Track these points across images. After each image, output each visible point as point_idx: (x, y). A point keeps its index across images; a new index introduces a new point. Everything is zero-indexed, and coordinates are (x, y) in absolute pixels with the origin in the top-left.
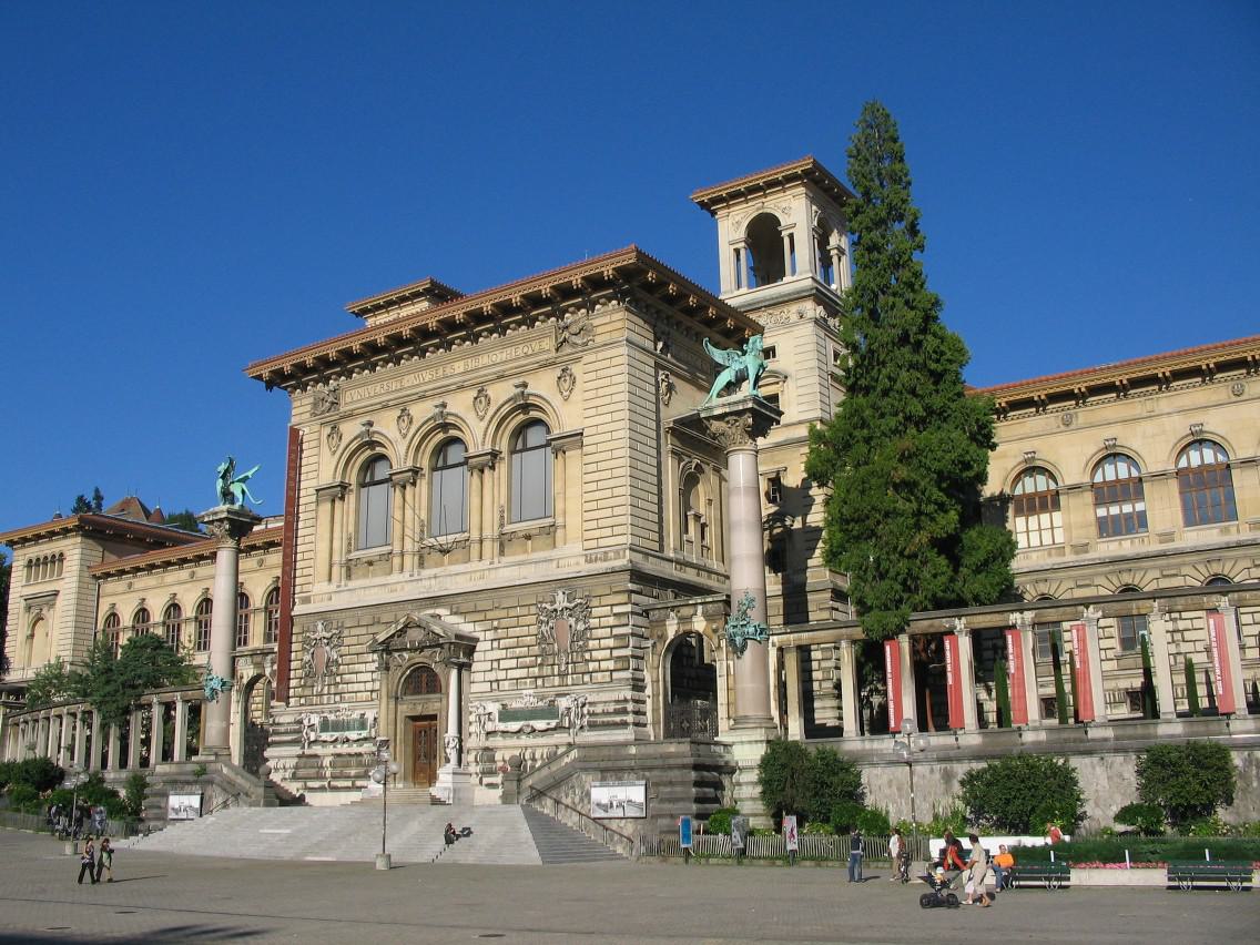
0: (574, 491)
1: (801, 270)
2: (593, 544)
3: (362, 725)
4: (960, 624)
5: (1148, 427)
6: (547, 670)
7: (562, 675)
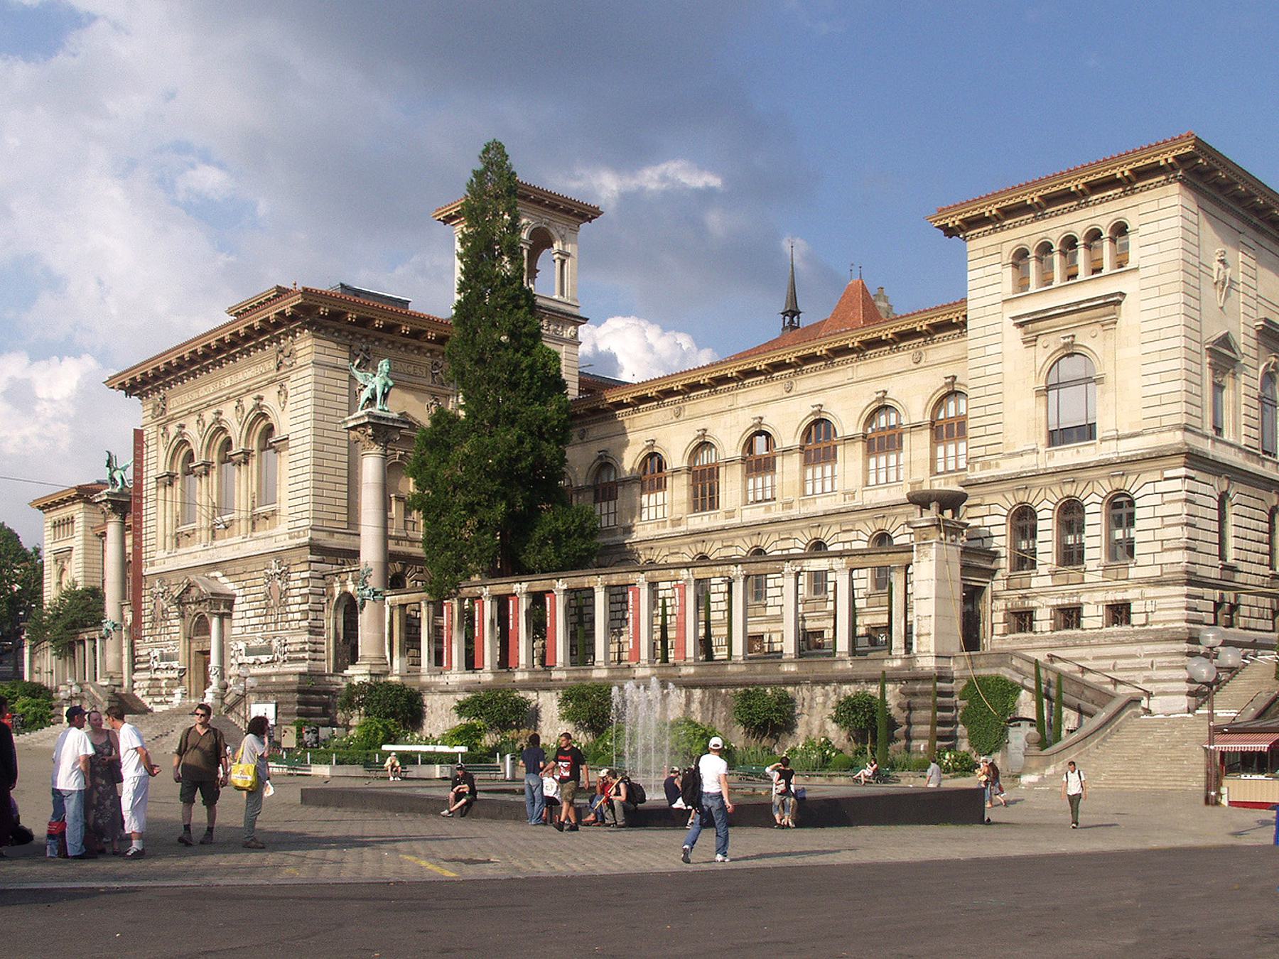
5: (728, 418)
6: (269, 619)
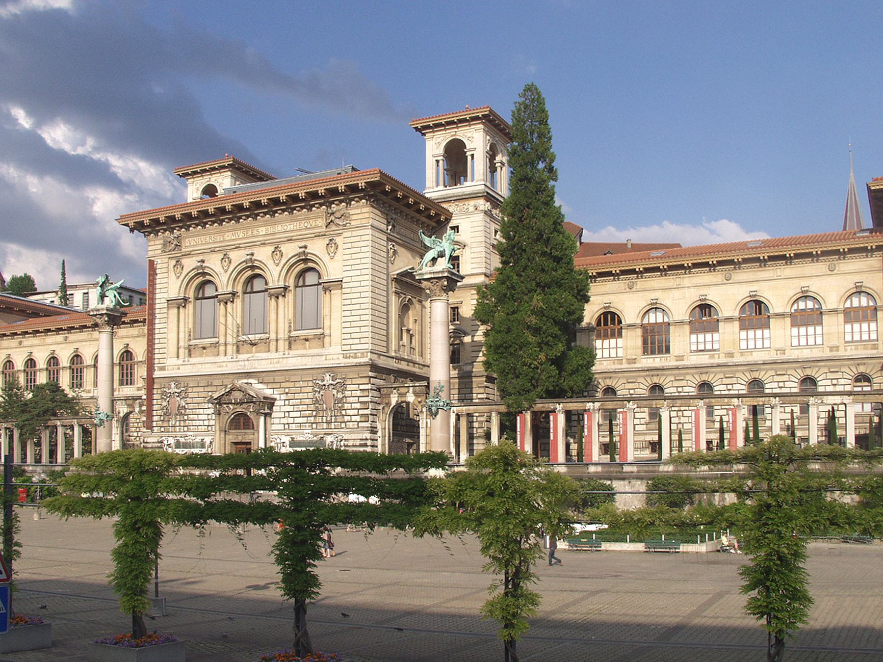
0: (336, 314)
1: (477, 178)
2: (348, 347)
3: (203, 446)
4: (559, 407)
5: (677, 293)
6: (319, 419)
7: (328, 423)
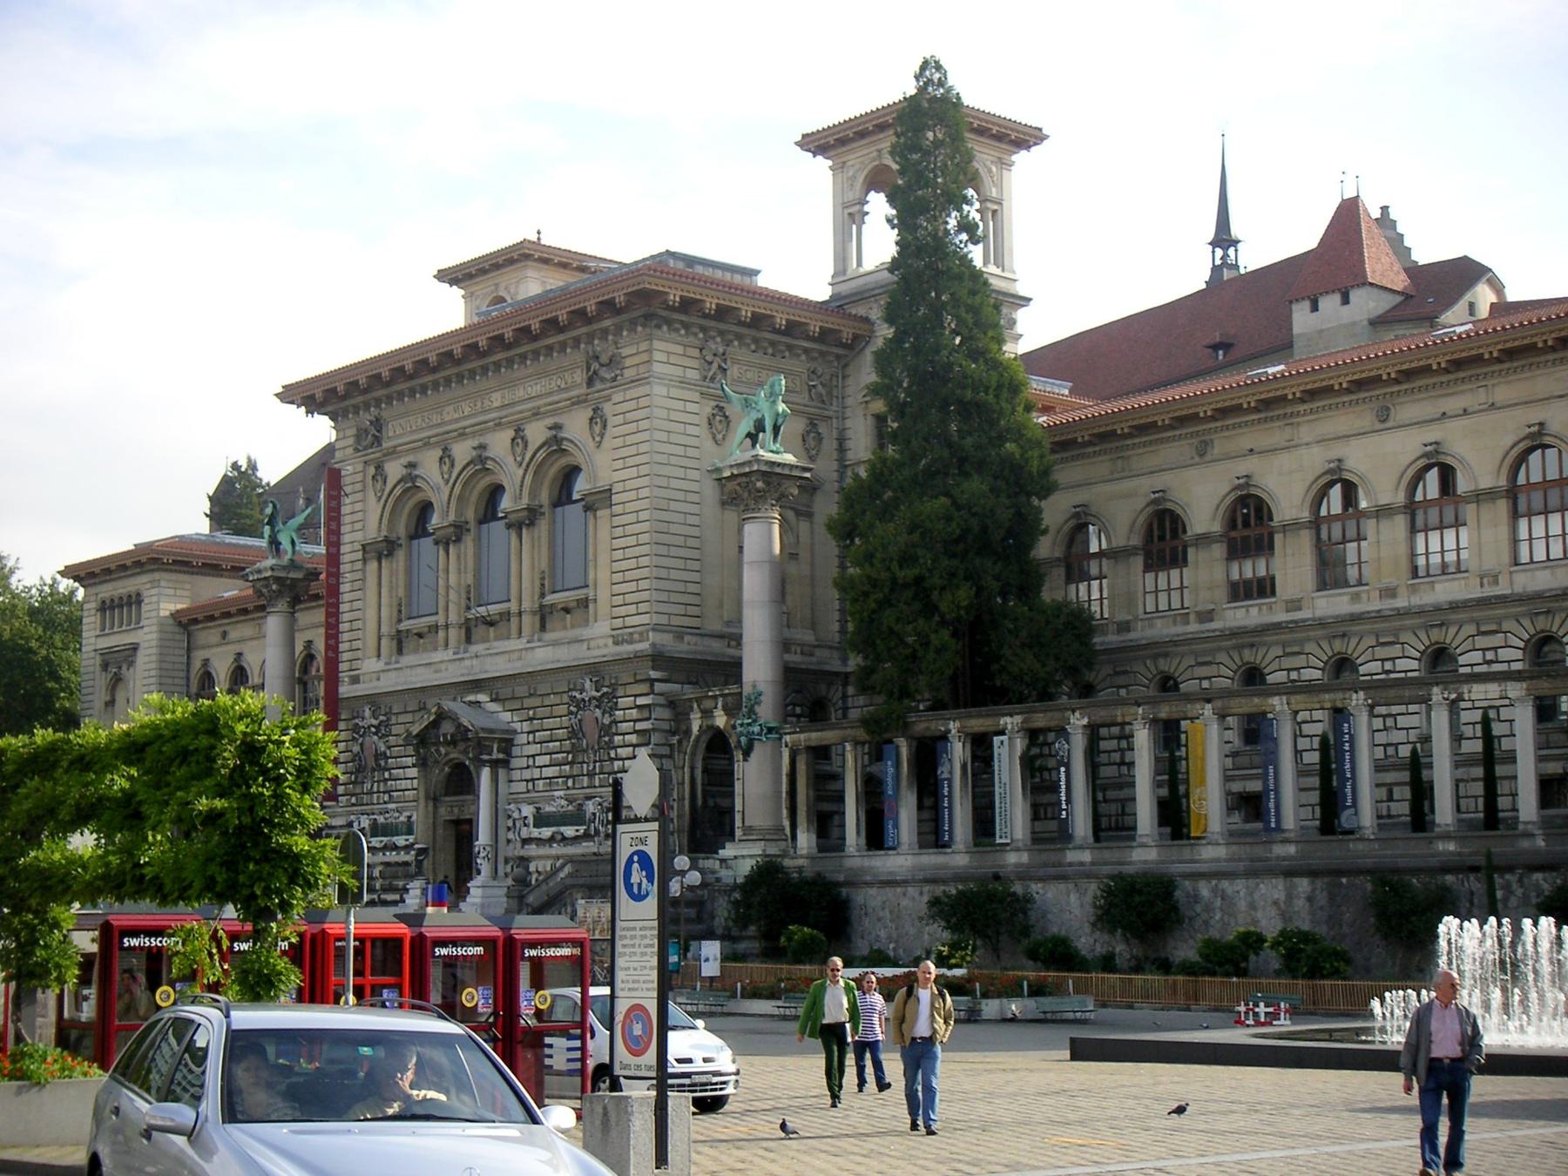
5: (1285, 460)
7: (591, 775)
